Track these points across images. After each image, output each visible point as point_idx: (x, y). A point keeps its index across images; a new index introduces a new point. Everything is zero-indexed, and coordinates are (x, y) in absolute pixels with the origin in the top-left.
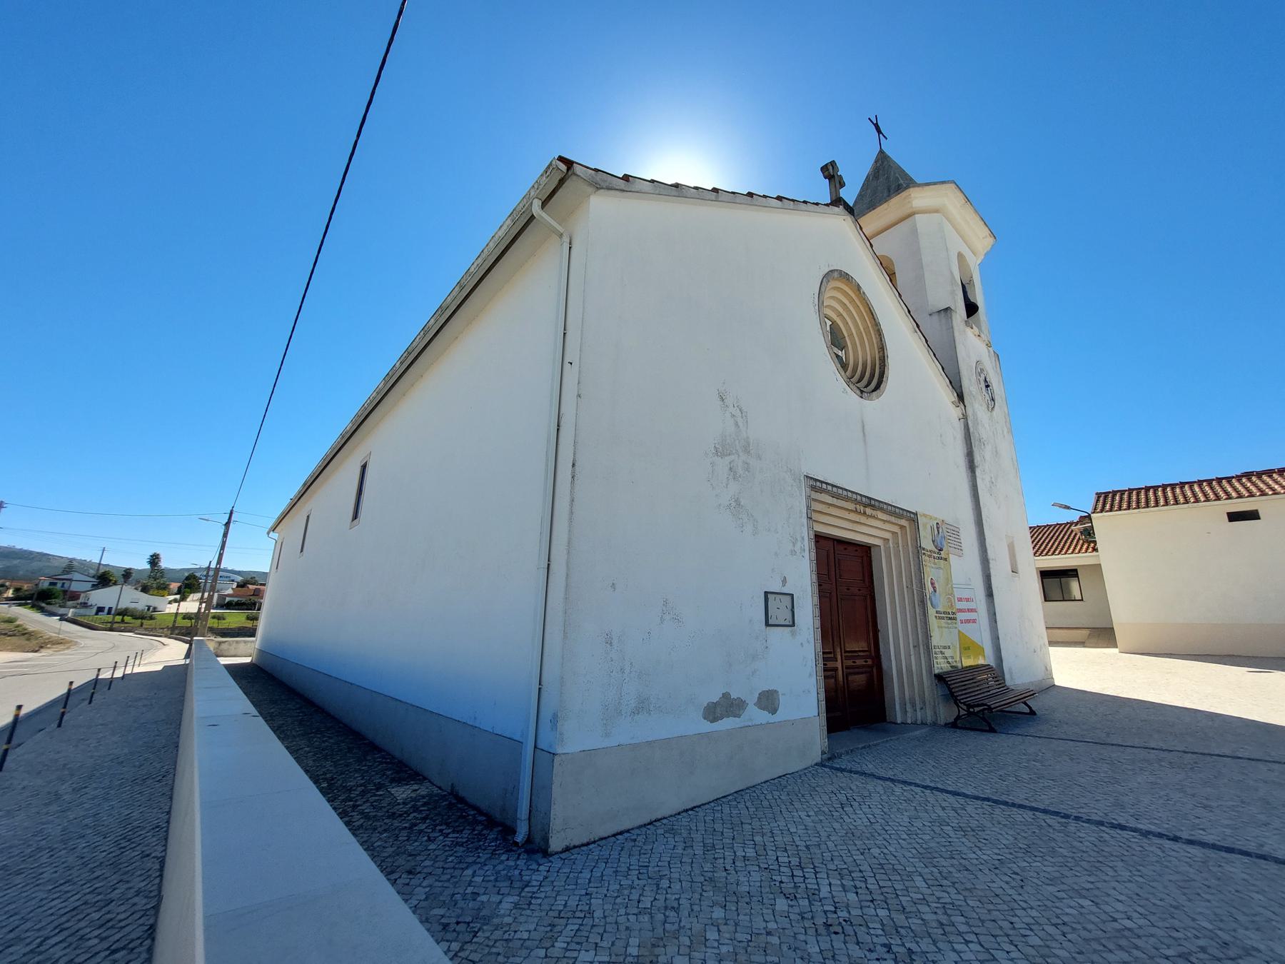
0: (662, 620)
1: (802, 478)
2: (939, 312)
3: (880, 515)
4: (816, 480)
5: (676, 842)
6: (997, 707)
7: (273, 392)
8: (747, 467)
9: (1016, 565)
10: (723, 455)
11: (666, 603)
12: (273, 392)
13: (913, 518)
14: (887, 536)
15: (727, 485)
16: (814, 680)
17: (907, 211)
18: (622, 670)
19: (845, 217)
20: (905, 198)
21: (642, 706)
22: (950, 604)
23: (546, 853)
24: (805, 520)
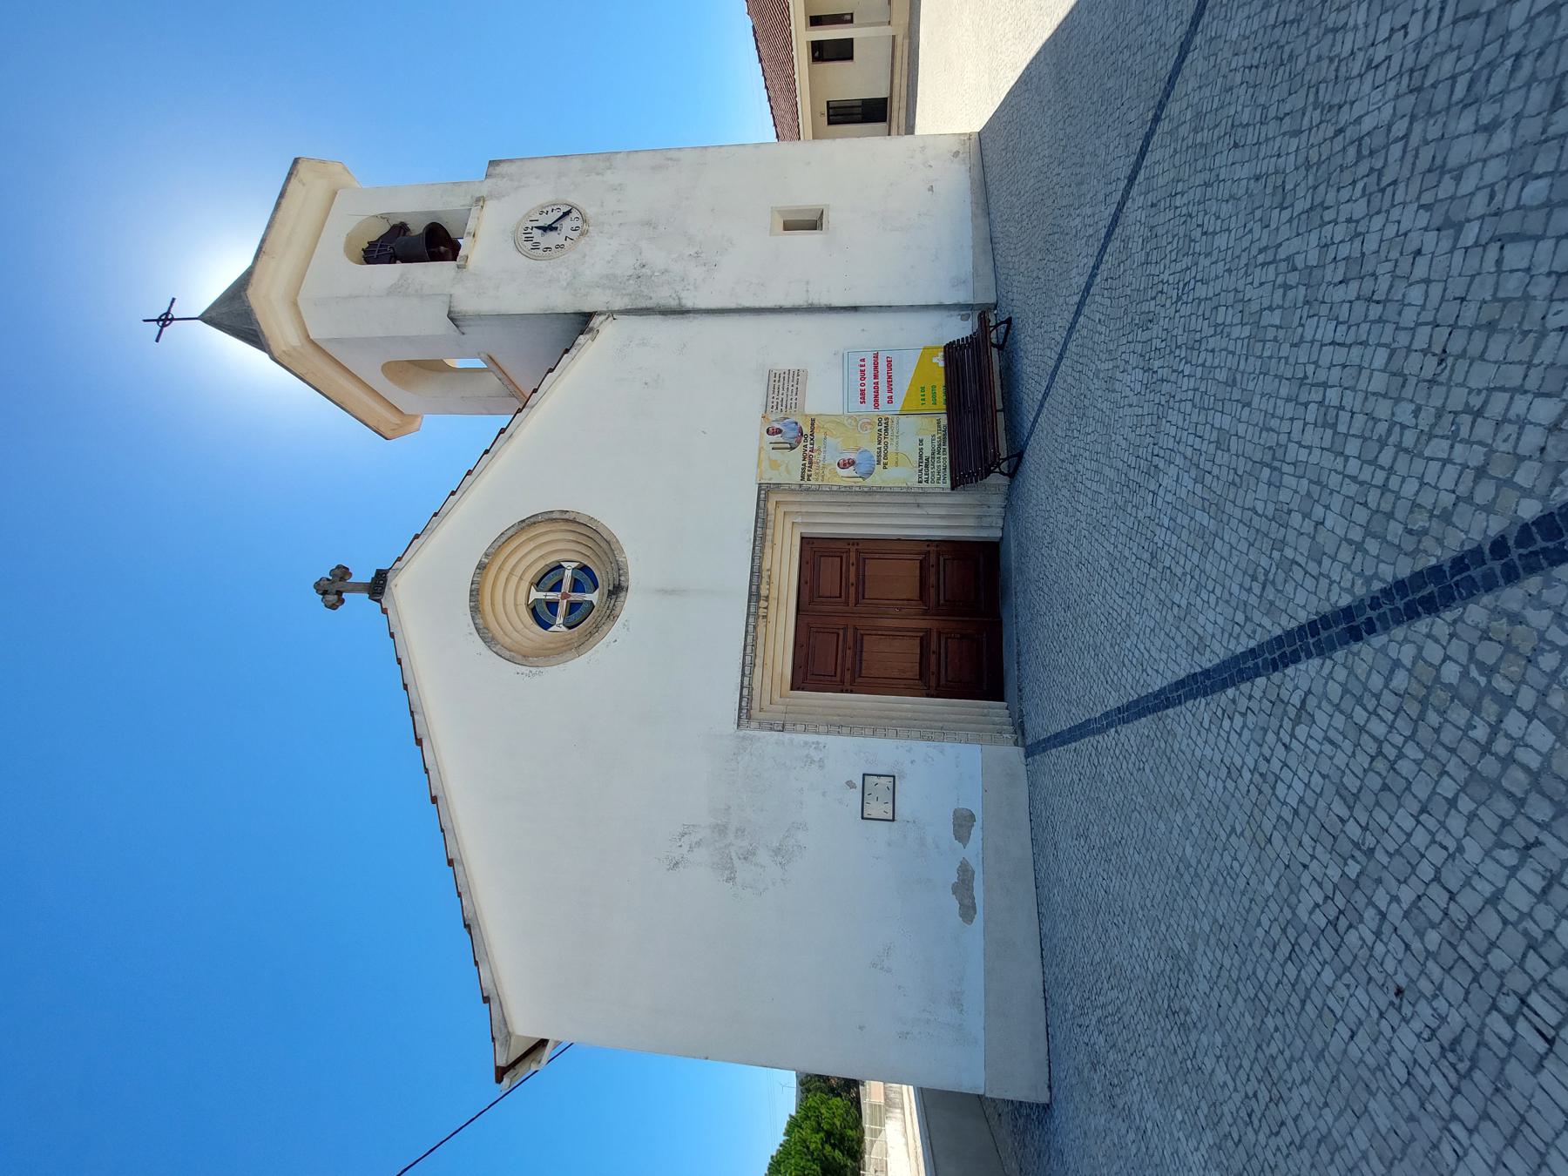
0: (889, 971)
1: (741, 733)
2: (457, 326)
3: (766, 565)
4: (739, 717)
5: (1322, 345)
6: (957, 527)
7: (811, 309)
8: (740, 831)
9: (811, 210)
10: (733, 870)
11: (874, 965)
12: (811, 309)
13: (765, 491)
14: (788, 526)
15: (762, 866)
16: (947, 746)
17: (309, 349)
18: (928, 1021)
19: (393, 587)
20: (290, 355)
21: (957, 1001)
22: (869, 427)
23: (1047, 1107)
24: (786, 736)
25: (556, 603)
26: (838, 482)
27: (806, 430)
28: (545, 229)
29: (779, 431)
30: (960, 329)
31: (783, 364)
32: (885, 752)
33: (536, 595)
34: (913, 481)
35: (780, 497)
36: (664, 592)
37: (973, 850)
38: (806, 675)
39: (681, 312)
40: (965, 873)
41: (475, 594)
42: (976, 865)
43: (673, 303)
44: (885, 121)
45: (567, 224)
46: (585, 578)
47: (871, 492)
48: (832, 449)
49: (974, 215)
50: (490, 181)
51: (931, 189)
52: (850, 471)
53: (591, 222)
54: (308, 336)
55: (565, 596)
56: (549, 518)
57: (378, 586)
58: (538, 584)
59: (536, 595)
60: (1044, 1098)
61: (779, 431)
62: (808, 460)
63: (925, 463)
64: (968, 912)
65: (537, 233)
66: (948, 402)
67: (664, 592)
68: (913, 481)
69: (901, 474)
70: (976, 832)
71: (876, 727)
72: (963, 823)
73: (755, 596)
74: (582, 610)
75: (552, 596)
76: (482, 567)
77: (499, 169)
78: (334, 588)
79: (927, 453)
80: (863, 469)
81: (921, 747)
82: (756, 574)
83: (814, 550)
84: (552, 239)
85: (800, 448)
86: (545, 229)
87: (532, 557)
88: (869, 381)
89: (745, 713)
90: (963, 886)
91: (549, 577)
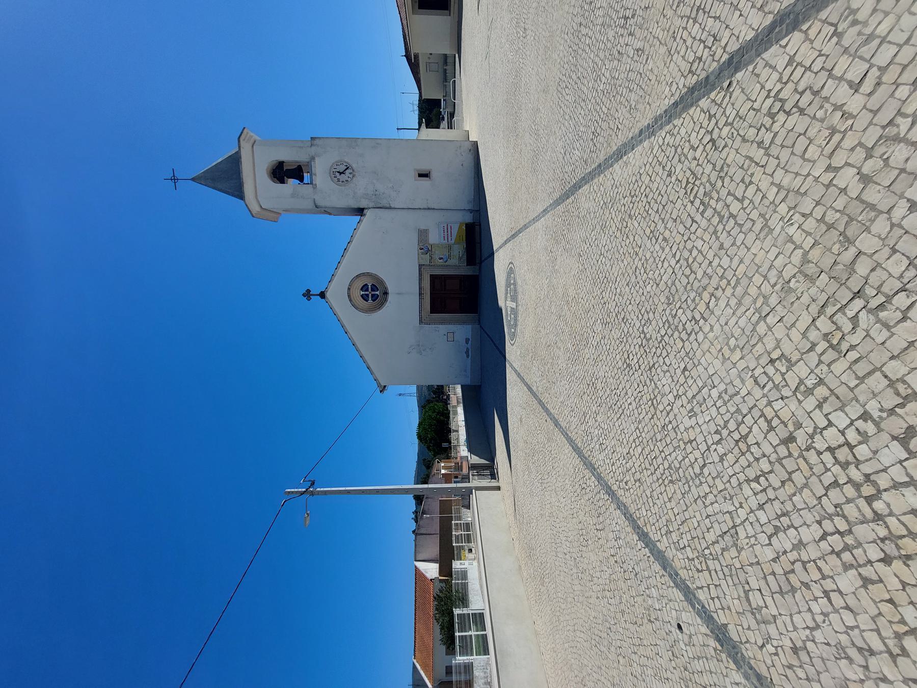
13: (420, 266)
21: (465, 371)
25: (368, 295)
26: (438, 264)
27: (430, 249)
28: (341, 173)
29: (422, 249)
30: (469, 218)
31: (422, 228)
32: (451, 328)
33: (362, 293)
34: (457, 263)
35: (424, 267)
36: (398, 294)
37: (469, 345)
38: (434, 310)
39: (390, 208)
40: (467, 348)
41: (349, 296)
42: (469, 348)
43: (388, 206)
44: (476, 312)
45: (347, 171)
46: (374, 288)
47: (447, 266)
48: (437, 254)
49: (474, 178)
50: (313, 148)
51: (462, 165)
52: (441, 261)
53: (355, 170)
54: (261, 207)
55: (370, 293)
56: (363, 274)
57: (322, 295)
58: (362, 289)
59: (362, 293)
60: (480, 384)
61: (422, 249)
62: (431, 257)
63: (460, 258)
64: (468, 356)
65: (338, 174)
66: (466, 240)
67: (398, 294)
68: (457, 263)
69: (454, 261)
70: (470, 342)
71: (450, 322)
72: (467, 341)
73: (420, 294)
74: (364, 289)
75: (366, 293)
76: (349, 289)
77: (317, 142)
78: (308, 294)
79: (461, 256)
80: (445, 260)
81: (459, 326)
82: (420, 288)
83: (433, 278)
84: (343, 177)
85: (428, 254)
86: (341, 173)
87: (359, 284)
88: (446, 233)
89: (421, 322)
90: (467, 352)
91: (364, 288)
